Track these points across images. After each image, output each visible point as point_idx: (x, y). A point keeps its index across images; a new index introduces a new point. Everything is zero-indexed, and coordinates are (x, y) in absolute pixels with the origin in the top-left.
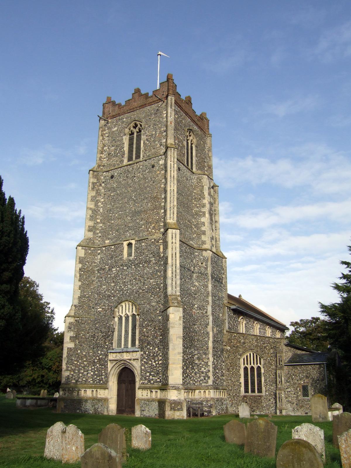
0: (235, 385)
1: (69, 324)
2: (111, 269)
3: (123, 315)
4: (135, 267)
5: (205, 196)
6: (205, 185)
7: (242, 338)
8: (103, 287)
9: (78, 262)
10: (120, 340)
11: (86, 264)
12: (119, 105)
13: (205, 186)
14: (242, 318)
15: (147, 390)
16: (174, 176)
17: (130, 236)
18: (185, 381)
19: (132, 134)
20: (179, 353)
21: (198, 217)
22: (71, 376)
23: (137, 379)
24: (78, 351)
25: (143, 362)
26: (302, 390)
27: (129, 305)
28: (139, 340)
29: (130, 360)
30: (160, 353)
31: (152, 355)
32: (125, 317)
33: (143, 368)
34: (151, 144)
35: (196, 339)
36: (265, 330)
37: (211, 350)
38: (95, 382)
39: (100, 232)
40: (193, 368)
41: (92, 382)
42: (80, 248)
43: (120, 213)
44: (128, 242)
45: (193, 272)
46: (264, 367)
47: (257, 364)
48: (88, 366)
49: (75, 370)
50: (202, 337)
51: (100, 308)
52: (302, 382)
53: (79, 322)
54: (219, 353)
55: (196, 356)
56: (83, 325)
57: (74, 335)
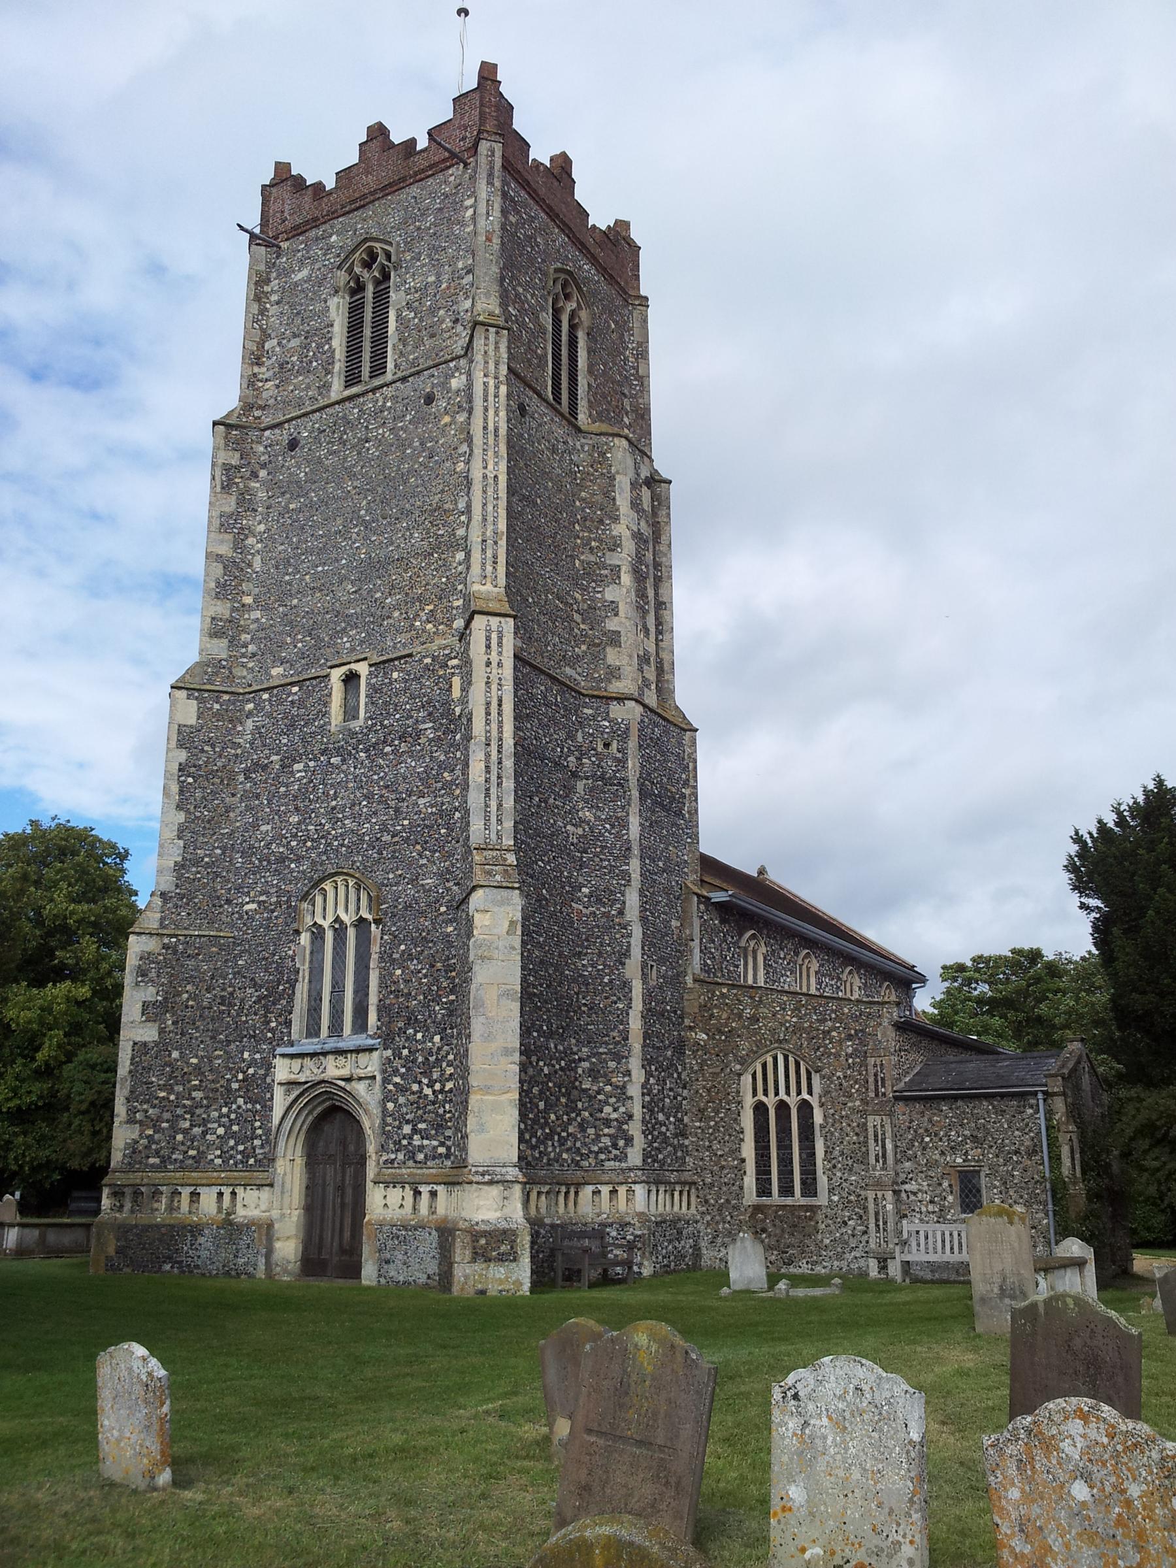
0: (723, 1167)
1: (141, 959)
2: (291, 766)
3: (326, 924)
4: (368, 757)
5: (618, 510)
6: (618, 473)
7: (747, 1000)
8: (264, 828)
9: (174, 743)
10: (314, 1010)
11: (202, 751)
12: (319, 186)
13: (618, 477)
14: (753, 937)
15: (403, 1187)
16: (496, 430)
17: (353, 649)
18: (540, 1152)
19: (359, 288)
20: (507, 1052)
21: (593, 584)
22: (144, 1142)
23: (371, 1148)
24: (170, 1055)
25: (390, 1087)
26: (956, 1189)
27: (347, 886)
28: (379, 1010)
29: (348, 1080)
30: (448, 1053)
31: (420, 1059)
32: (336, 930)
33: (390, 1106)
34: (421, 320)
35: (585, 1005)
36: (839, 979)
37: (636, 1043)
38: (231, 1162)
39: (252, 639)
40: (571, 1108)
41: (218, 1161)
42: (183, 694)
43: (320, 569)
44: (344, 669)
45: (574, 775)
46: (822, 1105)
47: (799, 1093)
48: (208, 1107)
49: (159, 1119)
50: (606, 998)
51: (253, 902)
52: (959, 1160)
53: (175, 952)
54: (669, 1053)
55: (586, 1065)
56: (191, 963)
57: (159, 998)
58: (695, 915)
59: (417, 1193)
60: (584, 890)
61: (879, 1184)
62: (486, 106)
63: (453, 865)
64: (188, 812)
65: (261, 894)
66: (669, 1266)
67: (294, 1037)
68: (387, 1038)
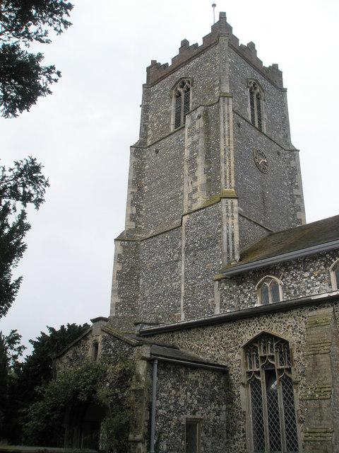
19: (180, 95)
62: (221, 29)
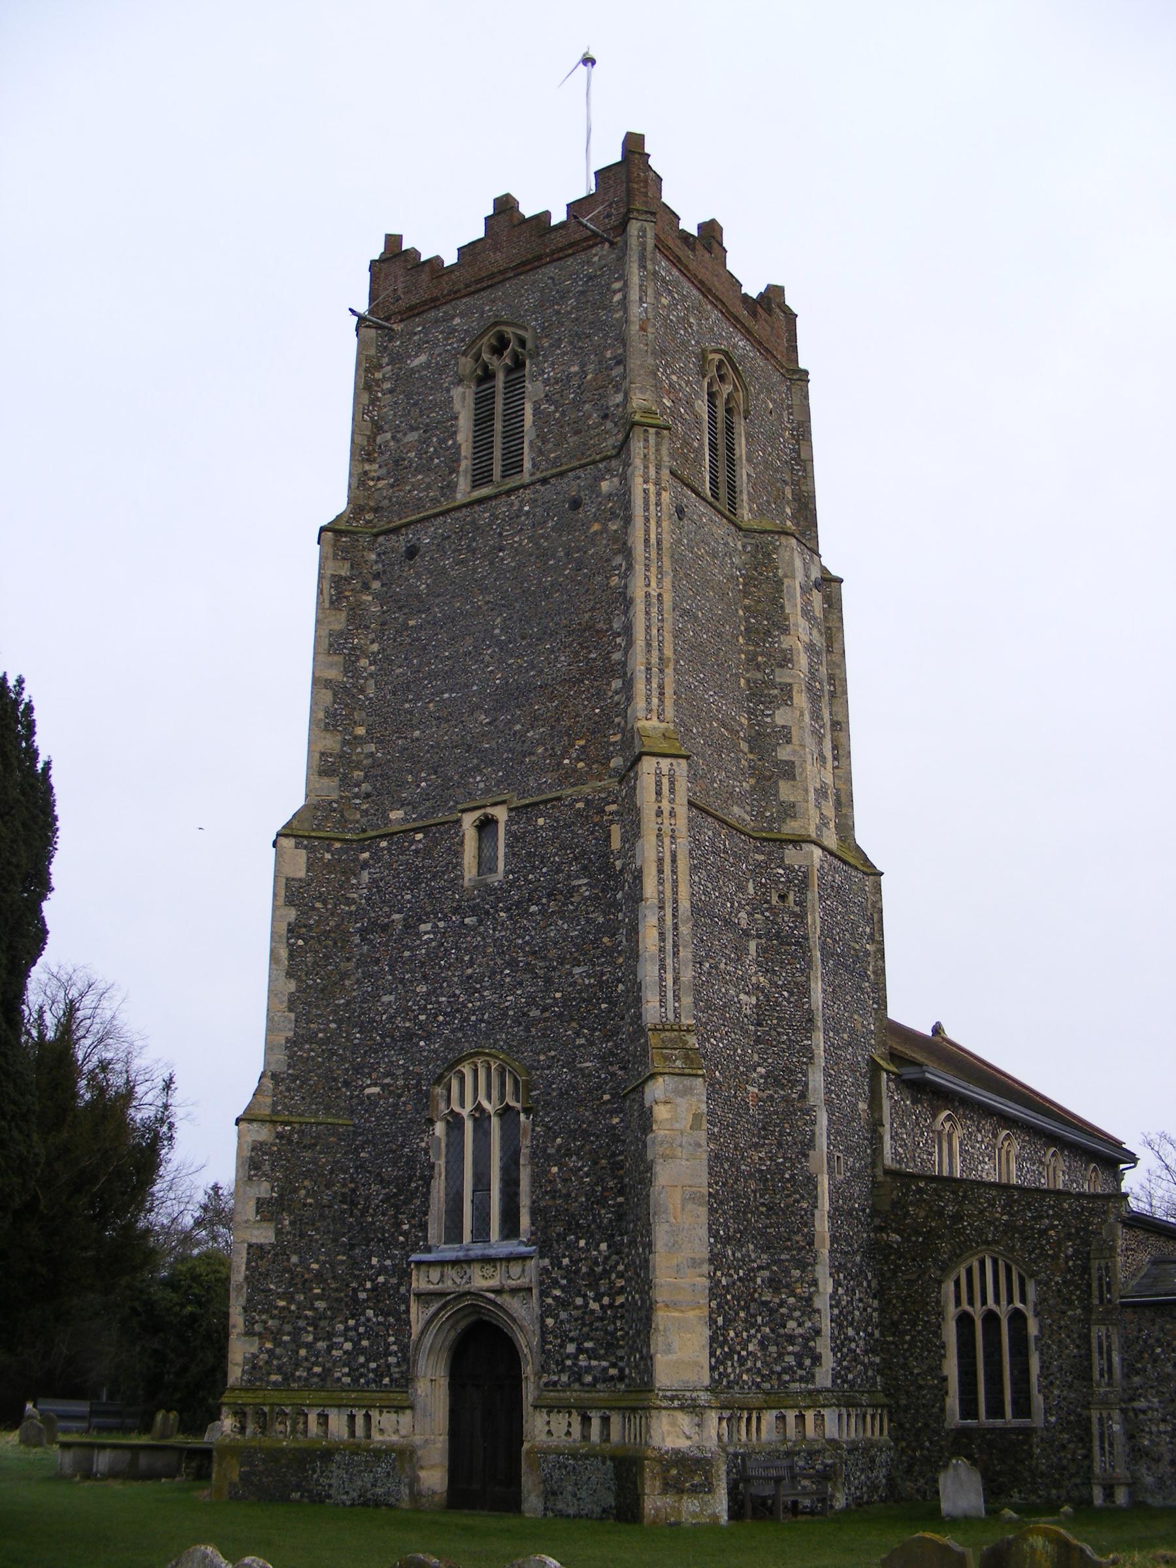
0: (920, 1387)
3: (465, 1113)
4: (510, 918)
5: (787, 619)
6: (786, 576)
9: (281, 900)
11: (313, 908)
13: (786, 581)
15: (570, 1414)
17: (487, 791)
18: (720, 1374)
19: (487, 376)
21: (761, 707)
22: (264, 1356)
23: (528, 1370)
24: (288, 1260)
29: (498, 1292)
30: (617, 1263)
31: (584, 1269)
33: (550, 1322)
34: (563, 414)
35: (763, 1204)
39: (366, 776)
43: (446, 696)
44: (477, 814)
47: (1010, 1300)
48: (332, 1319)
51: (375, 1085)
53: (290, 1141)
56: (307, 1155)
57: (275, 1195)
58: (884, 1095)
59: (586, 1421)
60: (759, 1069)
61: (1105, 1403)
62: (629, 180)
63: (616, 1046)
64: (299, 980)
65: (386, 1075)
66: (861, 1498)
67: (431, 1241)
68: (544, 1245)
